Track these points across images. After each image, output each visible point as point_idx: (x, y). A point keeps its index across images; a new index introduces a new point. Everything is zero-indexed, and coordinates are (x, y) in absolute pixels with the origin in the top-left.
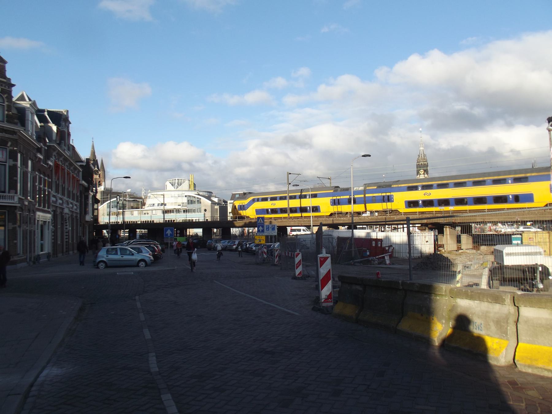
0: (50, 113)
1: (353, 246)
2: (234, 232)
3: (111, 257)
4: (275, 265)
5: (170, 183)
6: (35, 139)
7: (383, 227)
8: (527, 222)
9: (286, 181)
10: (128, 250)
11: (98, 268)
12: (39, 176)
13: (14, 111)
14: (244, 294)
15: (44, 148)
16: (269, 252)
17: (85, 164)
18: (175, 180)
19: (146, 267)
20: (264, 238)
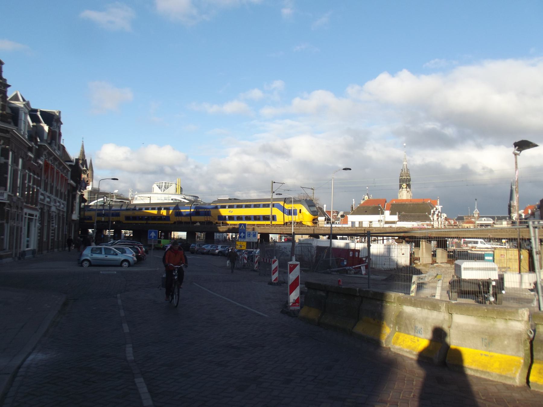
0: (42, 113)
1: (331, 255)
2: (218, 237)
3: (96, 256)
4: (255, 271)
5: (158, 186)
6: (27, 138)
7: (363, 238)
8: (502, 239)
9: (270, 190)
10: (112, 251)
11: (82, 266)
12: (29, 174)
13: (8, 111)
14: (221, 296)
15: (35, 147)
16: (250, 257)
17: (74, 164)
18: (162, 183)
19: (130, 268)
20: (245, 244)
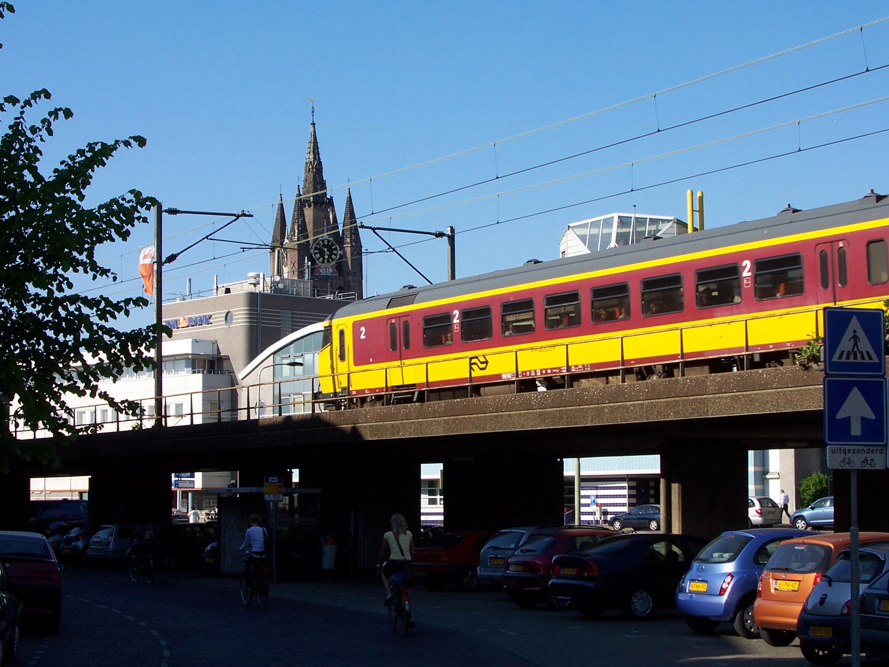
18: (608, 223)
